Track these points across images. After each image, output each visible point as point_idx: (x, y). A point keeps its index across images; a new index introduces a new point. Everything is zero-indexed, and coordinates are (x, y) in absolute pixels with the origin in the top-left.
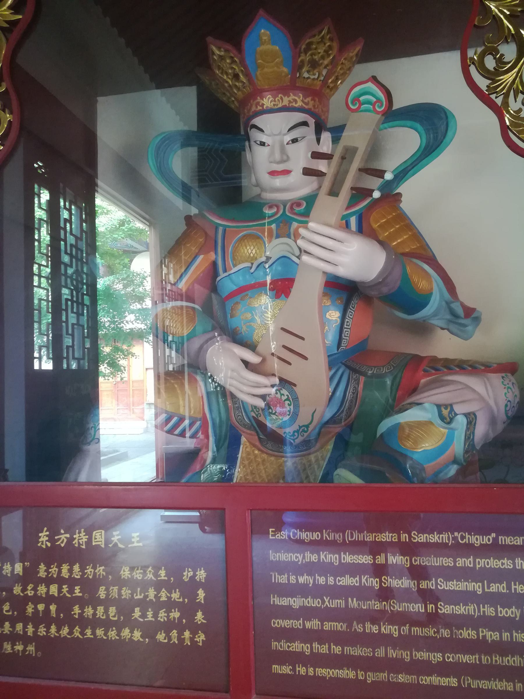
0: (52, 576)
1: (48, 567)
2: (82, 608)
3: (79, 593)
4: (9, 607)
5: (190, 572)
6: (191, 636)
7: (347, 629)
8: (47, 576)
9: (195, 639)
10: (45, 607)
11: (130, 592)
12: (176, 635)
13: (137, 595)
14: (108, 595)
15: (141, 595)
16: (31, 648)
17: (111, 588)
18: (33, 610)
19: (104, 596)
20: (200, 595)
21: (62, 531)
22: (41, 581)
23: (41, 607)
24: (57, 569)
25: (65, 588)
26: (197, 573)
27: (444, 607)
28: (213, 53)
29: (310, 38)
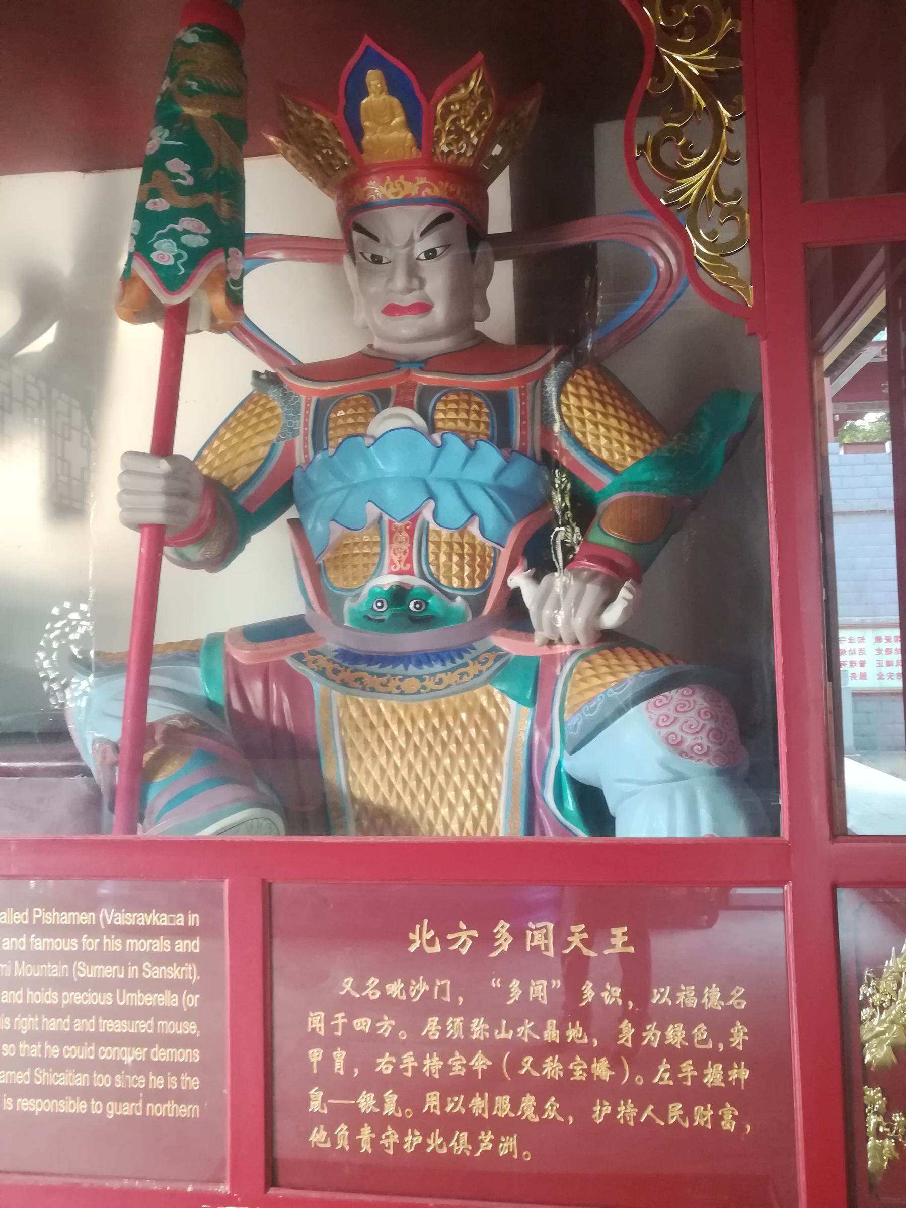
6: (374, 1135)
13: (499, 1033)
15: (507, 1032)
16: (508, 1145)
20: (735, 1035)
27: (151, 969)
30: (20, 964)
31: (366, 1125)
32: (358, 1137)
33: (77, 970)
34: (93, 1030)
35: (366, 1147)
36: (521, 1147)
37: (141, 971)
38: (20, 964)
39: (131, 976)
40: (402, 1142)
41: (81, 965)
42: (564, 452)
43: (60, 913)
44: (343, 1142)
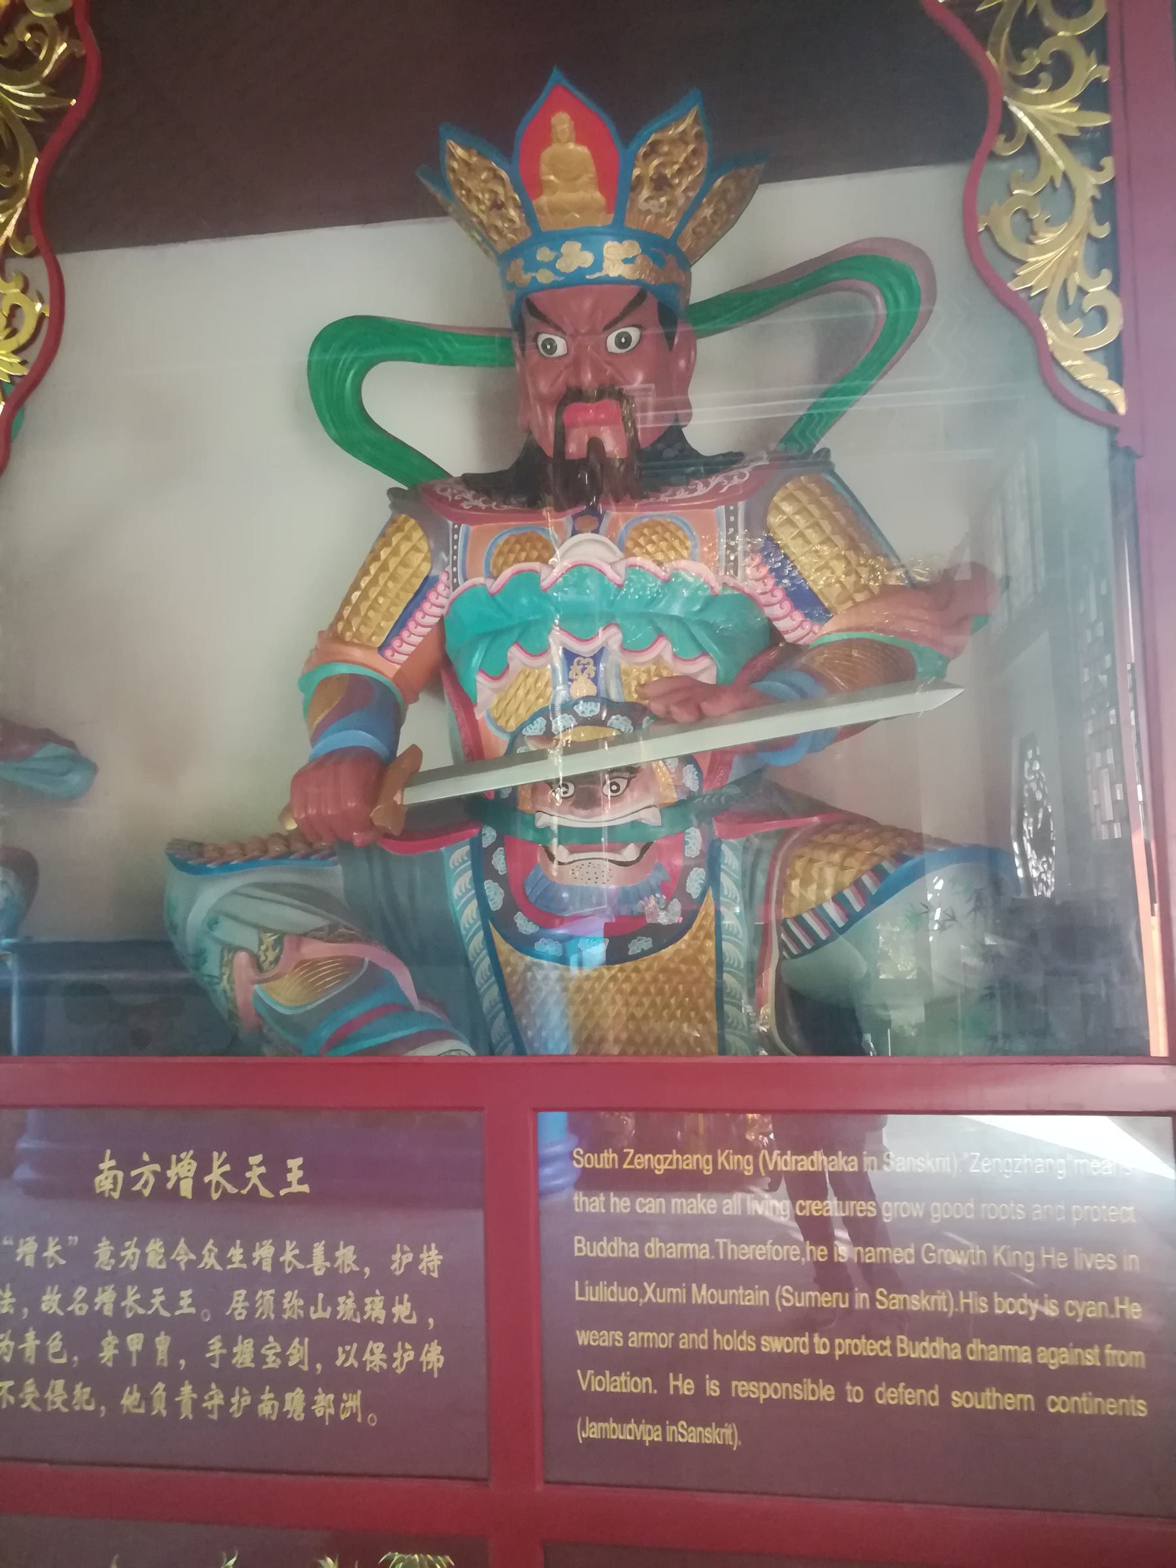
0: (127, 1265)
1: (118, 1247)
2: (229, 1343)
3: (189, 1306)
4: (61, 1344)
5: (406, 1252)
6: (195, 1396)
7: (312, 1365)
8: (115, 1267)
9: (204, 1405)
10: (145, 1340)
11: (301, 1302)
12: (164, 1394)
14: (251, 1310)
15: (324, 1310)
17: (260, 1293)
18: (116, 1352)
19: (245, 1312)
21: (146, 1157)
22: (105, 1278)
23: (135, 1342)
24: (138, 1251)
25: (132, 1295)
26: (422, 1256)
28: (452, 156)
29: (656, 131)
30: (699, 1289)
31: (187, 1382)
32: (177, 1399)
33: (781, 1297)
34: (706, 1347)
35: (186, 1412)
36: (366, 1406)
37: (873, 1299)
38: (699, 1289)
39: (858, 1305)
40: (228, 1404)
41: (787, 1291)
42: (270, 1030)
43: (666, 1244)
44: (160, 1407)
